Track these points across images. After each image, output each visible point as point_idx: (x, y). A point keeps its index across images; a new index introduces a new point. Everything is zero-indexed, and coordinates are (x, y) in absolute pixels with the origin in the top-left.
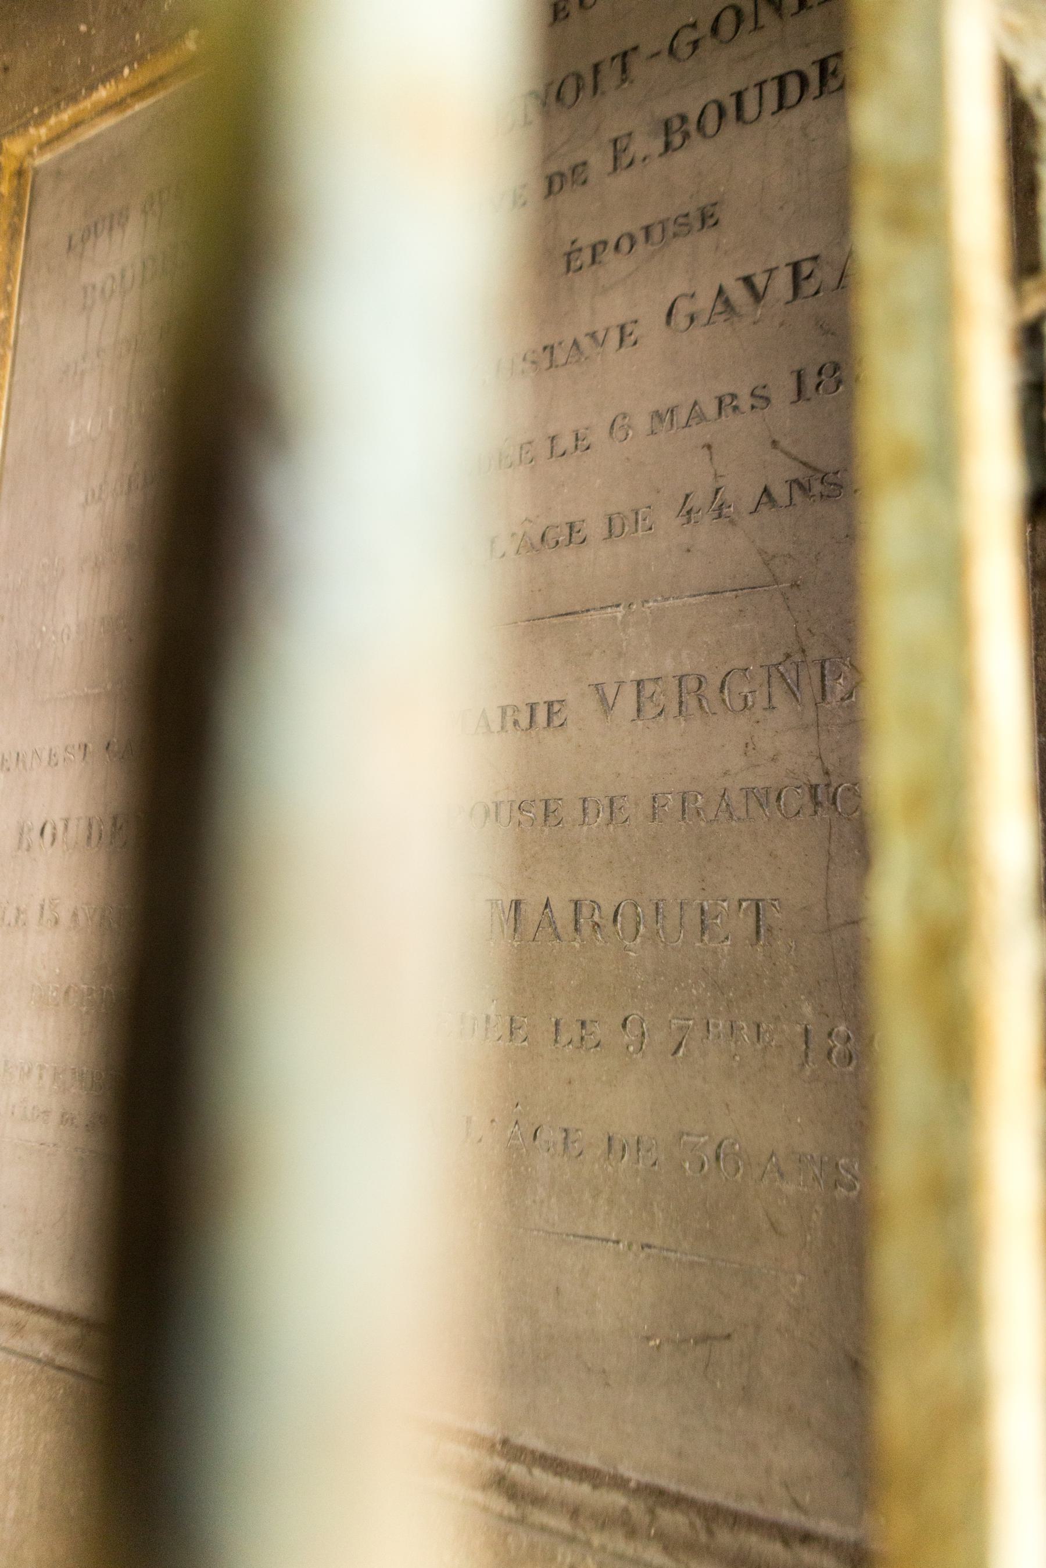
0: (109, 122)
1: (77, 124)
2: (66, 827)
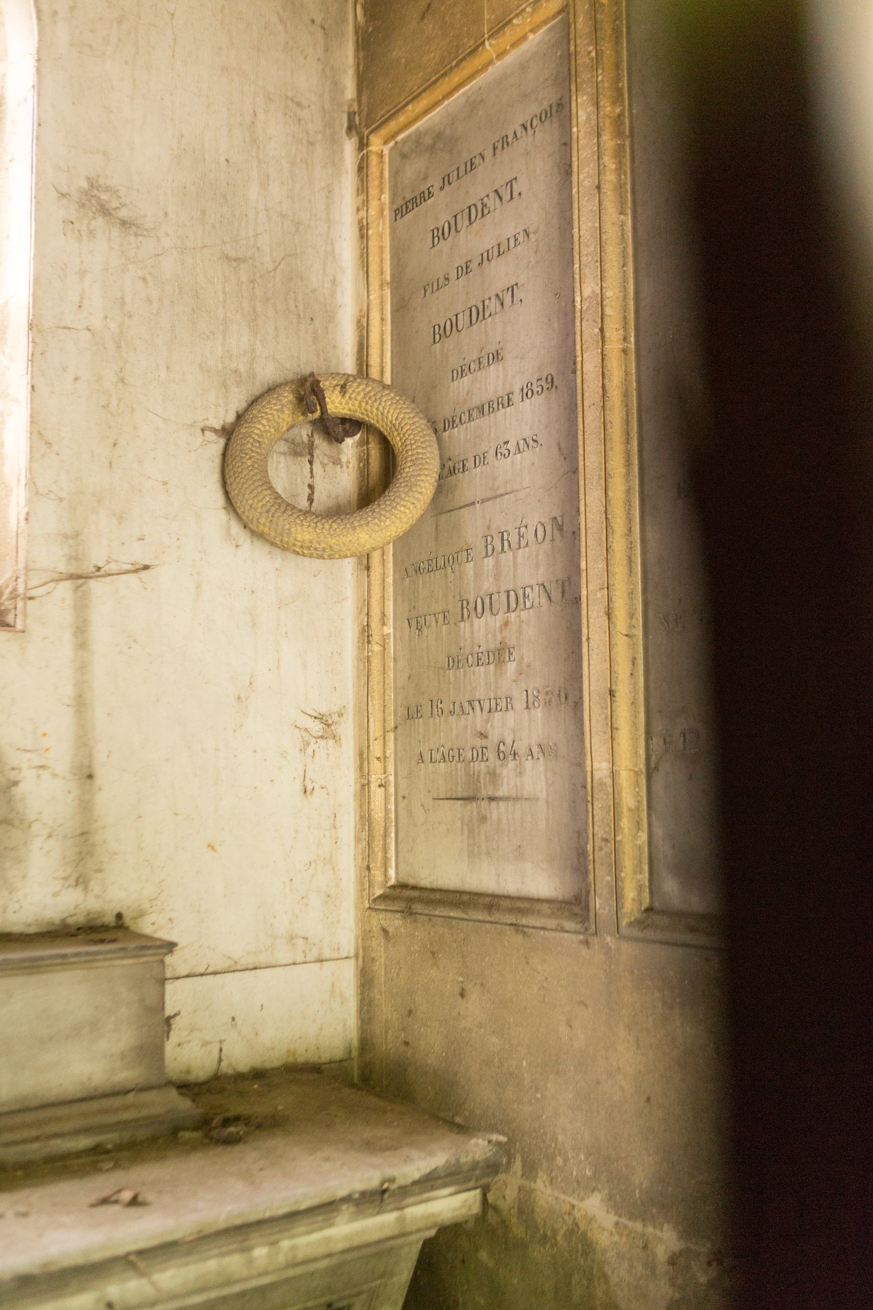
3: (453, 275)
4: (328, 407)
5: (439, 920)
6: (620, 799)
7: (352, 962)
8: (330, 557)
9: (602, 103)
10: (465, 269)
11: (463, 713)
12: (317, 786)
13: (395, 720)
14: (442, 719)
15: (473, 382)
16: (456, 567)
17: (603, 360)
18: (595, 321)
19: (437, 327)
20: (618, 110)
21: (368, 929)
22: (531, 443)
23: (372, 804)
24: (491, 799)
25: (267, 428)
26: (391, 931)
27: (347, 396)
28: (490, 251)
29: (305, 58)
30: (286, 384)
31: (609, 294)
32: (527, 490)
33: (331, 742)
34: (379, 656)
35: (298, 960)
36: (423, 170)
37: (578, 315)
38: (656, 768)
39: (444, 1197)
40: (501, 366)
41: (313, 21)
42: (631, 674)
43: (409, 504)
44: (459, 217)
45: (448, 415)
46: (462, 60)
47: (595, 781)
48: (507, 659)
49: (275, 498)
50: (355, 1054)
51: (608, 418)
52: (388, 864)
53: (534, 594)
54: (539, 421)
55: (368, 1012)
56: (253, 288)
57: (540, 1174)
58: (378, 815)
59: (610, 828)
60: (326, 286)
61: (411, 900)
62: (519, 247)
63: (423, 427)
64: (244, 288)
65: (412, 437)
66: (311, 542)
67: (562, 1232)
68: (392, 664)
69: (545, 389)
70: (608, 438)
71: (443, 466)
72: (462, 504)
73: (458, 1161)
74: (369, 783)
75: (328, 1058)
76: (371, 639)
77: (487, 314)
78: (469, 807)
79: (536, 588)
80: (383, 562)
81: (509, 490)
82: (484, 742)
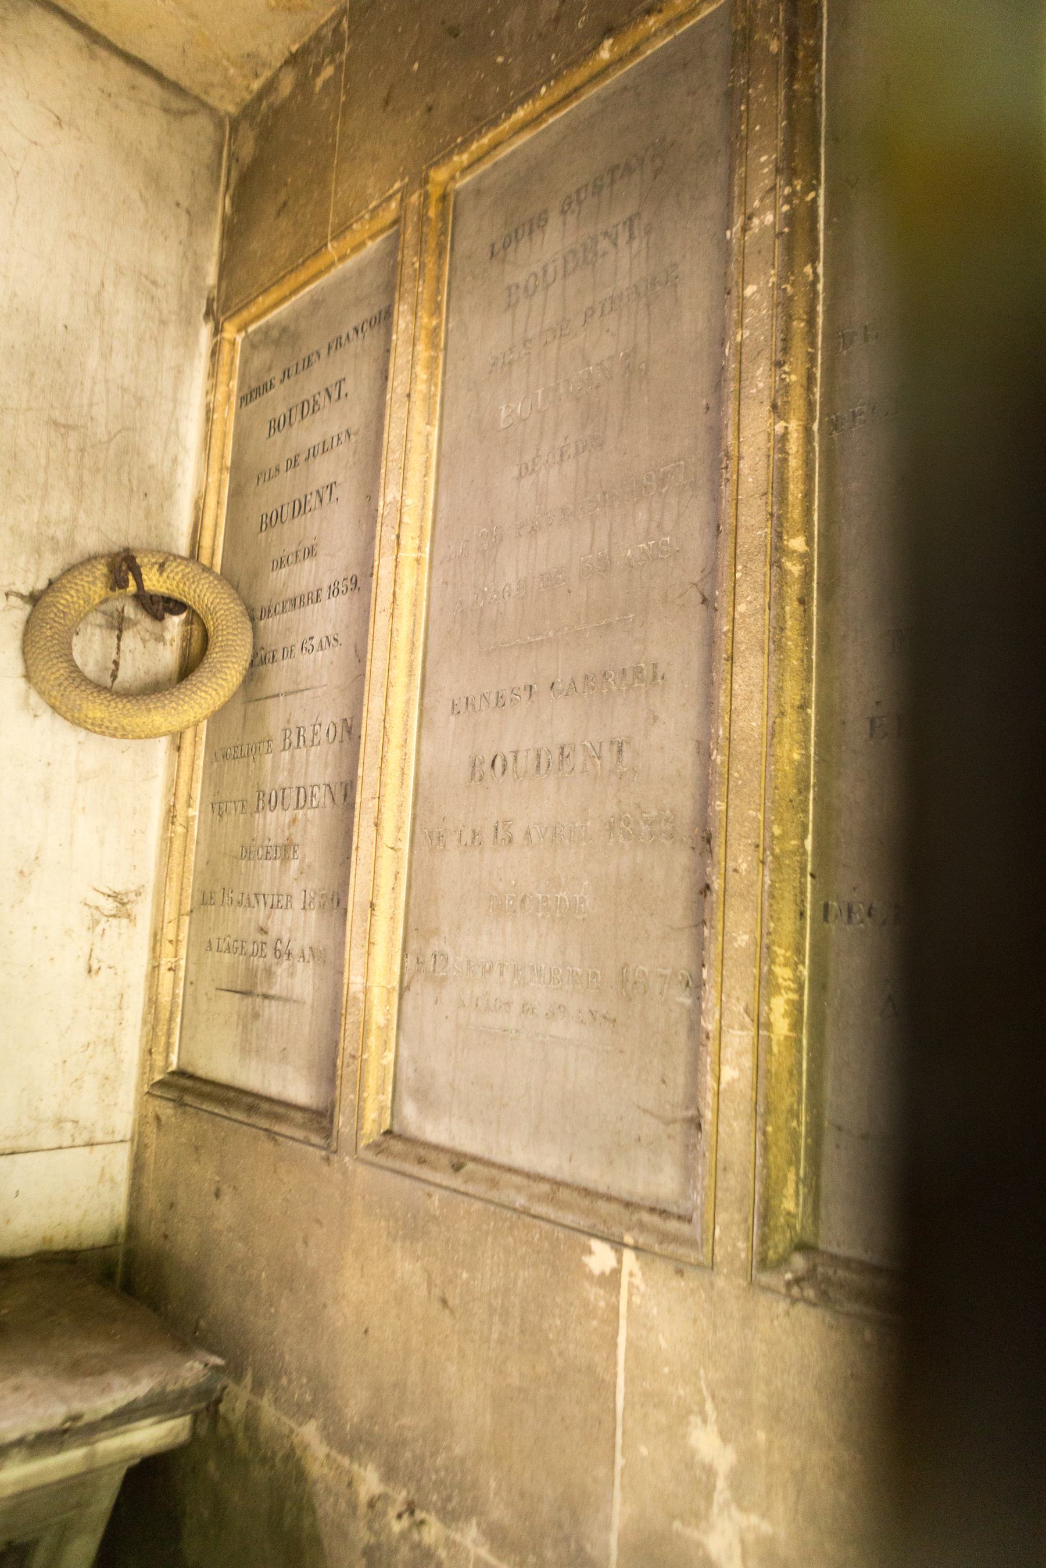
0: (526, 137)
1: (496, 146)
2: (516, 759)
3: (283, 467)
4: (144, 583)
5: (206, 1115)
6: (370, 1017)
7: (128, 1145)
8: (123, 736)
9: (420, 314)
10: (294, 463)
11: (249, 906)
12: (104, 966)
13: (192, 904)
14: (232, 908)
15: (289, 575)
16: (257, 757)
17: (396, 567)
18: (393, 527)
19: (264, 517)
20: (434, 323)
21: (145, 1114)
22: (332, 641)
23: (160, 987)
24: (266, 996)
25: (75, 599)
26: (163, 1118)
27: (165, 575)
28: (316, 448)
29: (166, 239)
30: (103, 556)
31: (408, 501)
32: (325, 688)
33: (124, 921)
34: (182, 838)
35: (65, 1144)
36: (268, 362)
37: (379, 519)
38: (408, 988)
39: (145, 1427)
40: (314, 562)
41: (178, 204)
42: (393, 889)
43: (210, 690)
44: (293, 411)
45: (266, 604)
46: (308, 258)
47: (350, 995)
48: (292, 857)
49: (71, 672)
50: (121, 1239)
51: (395, 626)
52: (170, 1050)
53: (321, 794)
54: (341, 621)
55: (137, 1198)
56: (83, 456)
57: (267, 1391)
58: (165, 999)
59: (358, 1045)
60: (166, 463)
61: (185, 1090)
62: (341, 447)
63: (237, 613)
64: (72, 455)
65: (224, 623)
66: (102, 720)
67: (280, 1454)
68: (194, 847)
69: (349, 589)
70: (393, 645)
71: (255, 655)
72: (269, 694)
73: (164, 1388)
74: (158, 966)
75: (91, 1243)
76: (175, 820)
77: (308, 509)
78: (245, 1002)
79: (323, 788)
80: (195, 744)
81: (309, 686)
82: (264, 938)
